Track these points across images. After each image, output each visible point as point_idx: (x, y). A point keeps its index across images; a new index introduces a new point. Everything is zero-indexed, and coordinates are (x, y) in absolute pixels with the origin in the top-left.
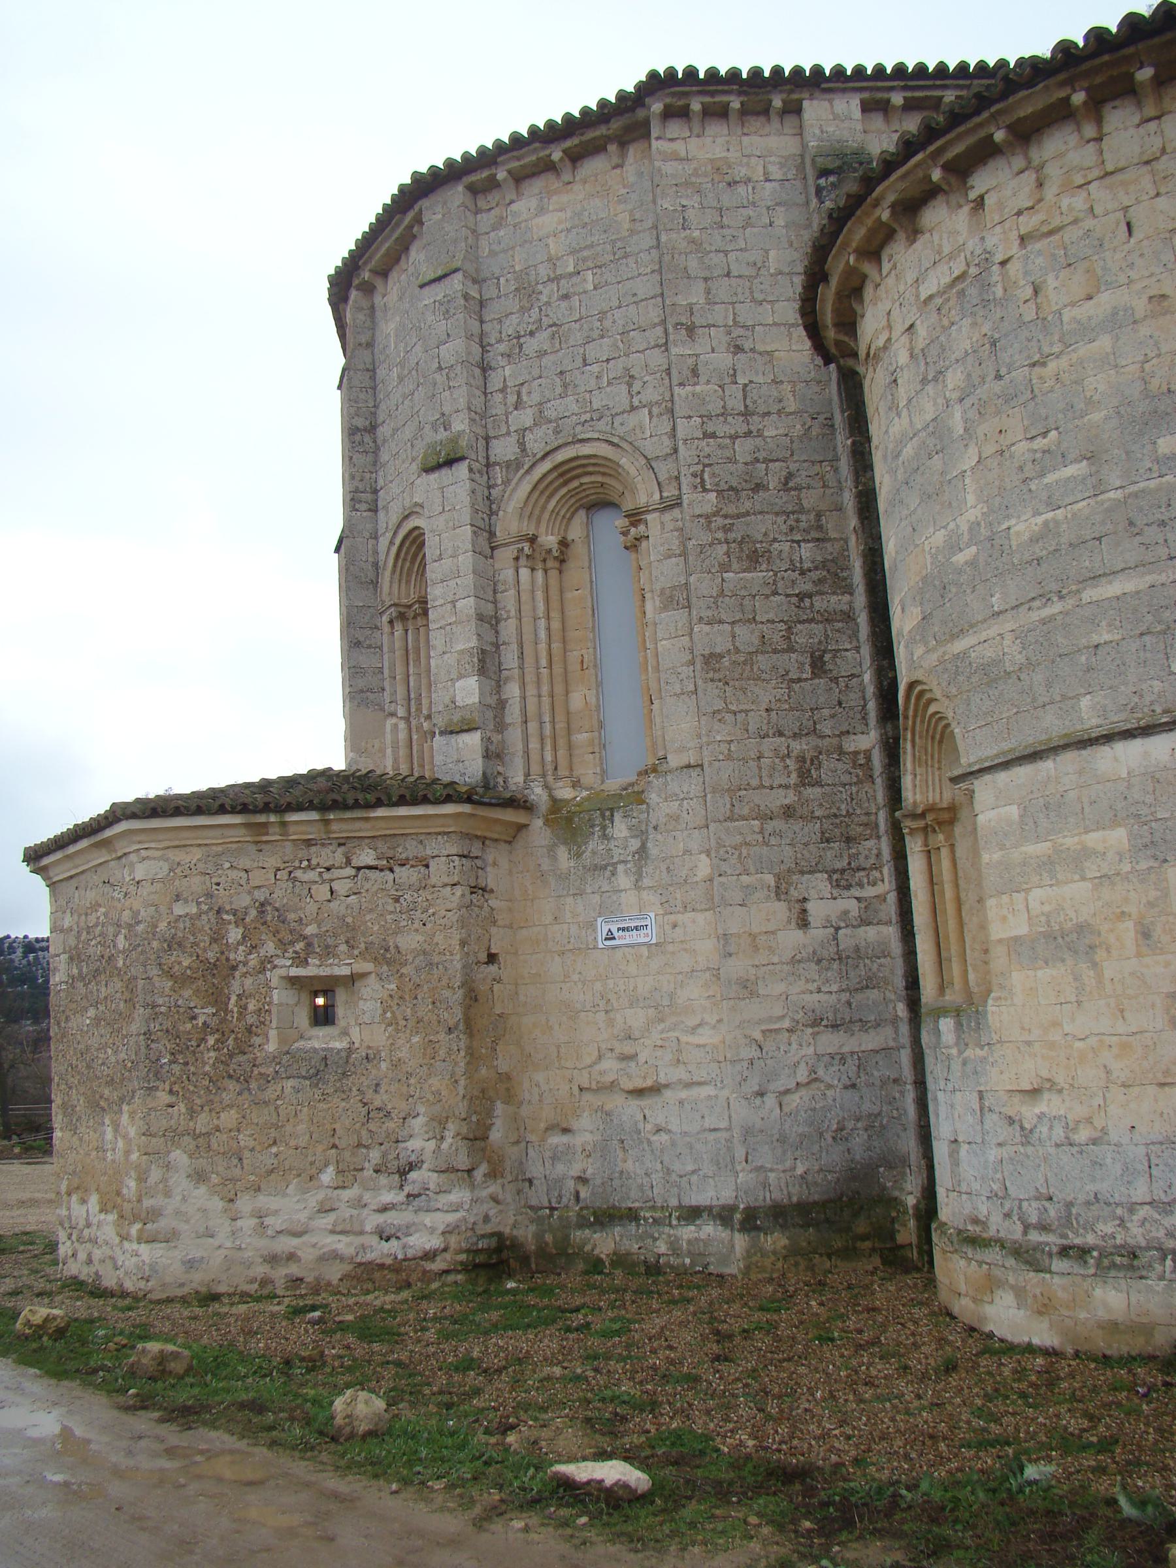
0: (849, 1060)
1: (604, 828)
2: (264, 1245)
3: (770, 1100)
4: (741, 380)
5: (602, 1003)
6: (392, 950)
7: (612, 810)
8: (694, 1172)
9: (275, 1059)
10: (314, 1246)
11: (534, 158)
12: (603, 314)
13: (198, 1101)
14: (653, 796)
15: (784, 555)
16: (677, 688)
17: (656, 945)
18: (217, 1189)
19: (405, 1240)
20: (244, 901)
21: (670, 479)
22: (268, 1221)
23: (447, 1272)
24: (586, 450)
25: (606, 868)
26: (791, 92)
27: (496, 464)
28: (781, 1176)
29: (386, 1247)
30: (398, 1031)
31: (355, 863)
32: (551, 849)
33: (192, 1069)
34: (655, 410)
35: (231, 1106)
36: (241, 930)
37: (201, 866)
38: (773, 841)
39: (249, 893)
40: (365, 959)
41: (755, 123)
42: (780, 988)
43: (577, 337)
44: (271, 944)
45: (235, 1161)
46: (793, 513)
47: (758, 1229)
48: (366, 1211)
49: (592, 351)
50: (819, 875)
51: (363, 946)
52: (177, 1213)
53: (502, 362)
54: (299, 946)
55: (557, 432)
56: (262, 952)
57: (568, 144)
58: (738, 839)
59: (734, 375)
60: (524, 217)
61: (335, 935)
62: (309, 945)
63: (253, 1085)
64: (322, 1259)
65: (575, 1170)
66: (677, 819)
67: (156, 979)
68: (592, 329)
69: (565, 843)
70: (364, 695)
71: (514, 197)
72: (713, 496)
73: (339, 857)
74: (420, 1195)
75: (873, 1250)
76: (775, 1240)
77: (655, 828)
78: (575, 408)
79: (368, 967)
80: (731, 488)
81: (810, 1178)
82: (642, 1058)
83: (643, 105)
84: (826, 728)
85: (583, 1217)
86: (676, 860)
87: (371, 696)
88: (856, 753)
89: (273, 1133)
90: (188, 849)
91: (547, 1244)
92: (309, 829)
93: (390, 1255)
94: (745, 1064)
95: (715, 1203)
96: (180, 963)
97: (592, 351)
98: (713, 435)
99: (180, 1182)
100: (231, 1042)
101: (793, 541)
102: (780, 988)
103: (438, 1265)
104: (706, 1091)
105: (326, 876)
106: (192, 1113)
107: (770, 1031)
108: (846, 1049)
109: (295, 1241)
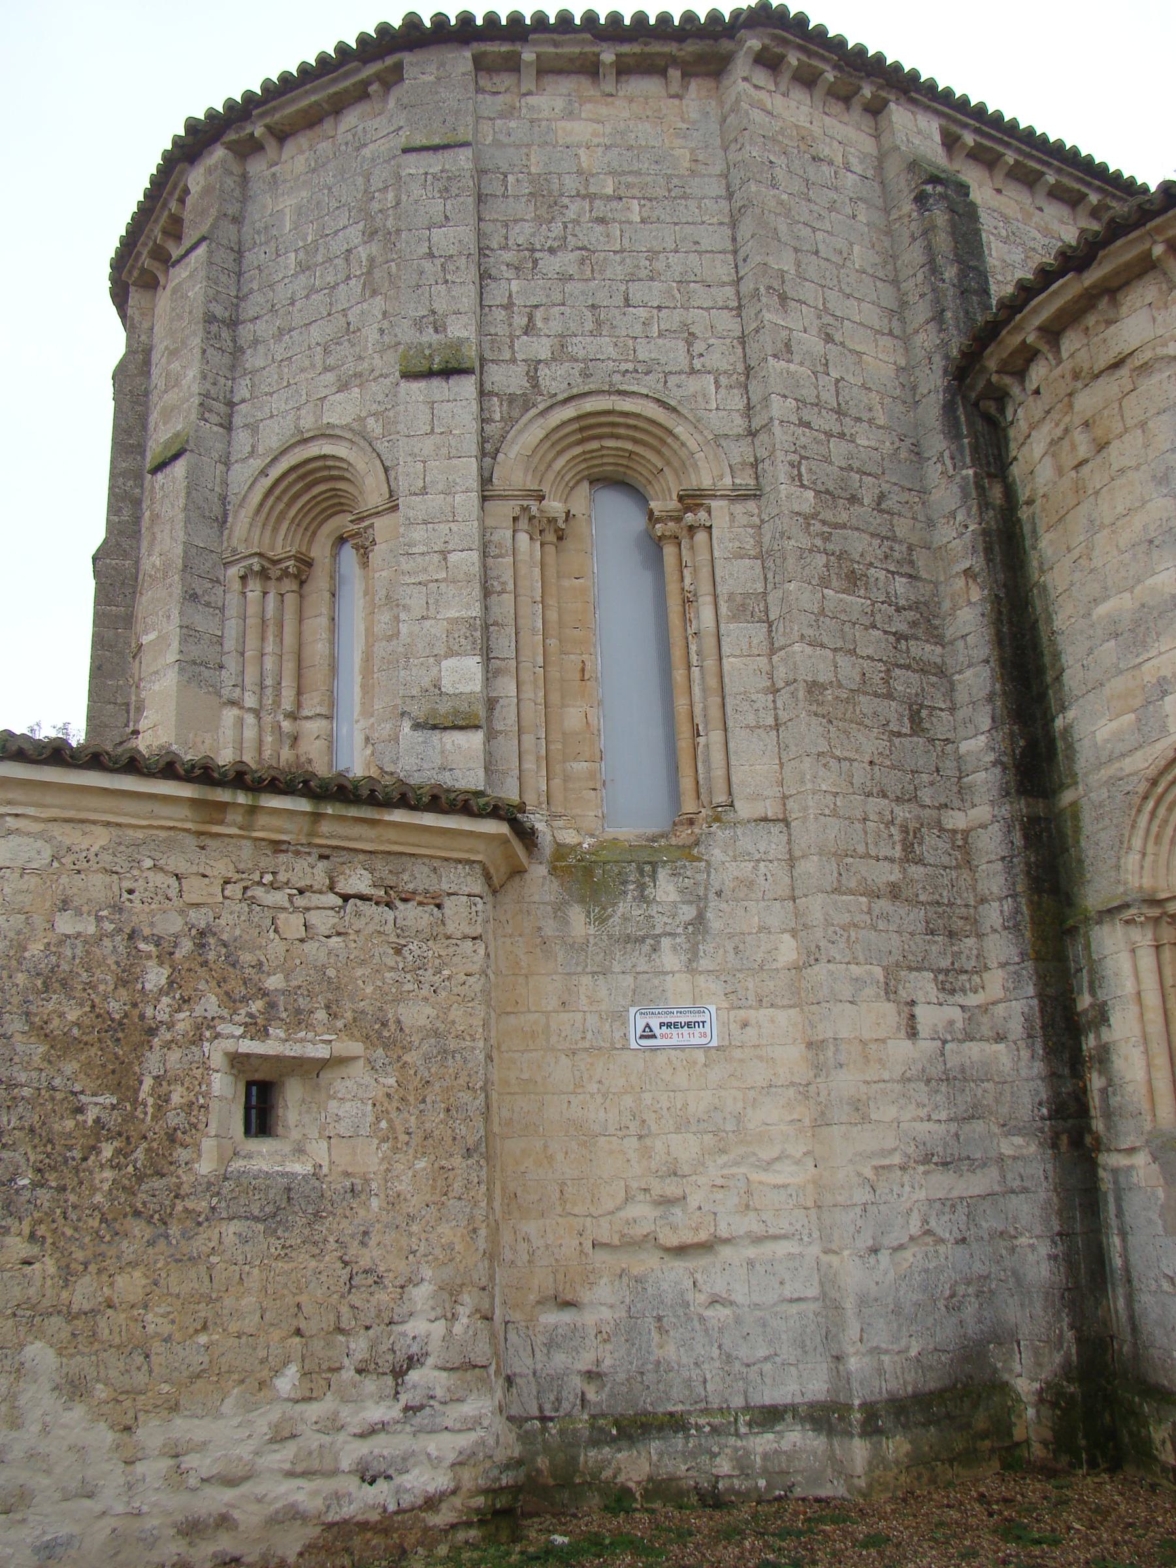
0: (959, 1207)
1: (642, 887)
2: (179, 1504)
3: (884, 1257)
4: (835, 374)
5: (634, 1127)
6: (392, 1026)
7: (654, 865)
8: (766, 1359)
9: (210, 1187)
10: (259, 1500)
11: (577, 50)
12: (652, 255)
13: (79, 1255)
14: (717, 852)
15: (881, 585)
16: (751, 719)
17: (717, 1049)
18: (105, 1409)
19: (398, 1480)
20: (172, 924)
21: (743, 463)
22: (190, 1461)
23: (453, 1527)
24: (627, 405)
25: (644, 940)
26: (880, 87)
27: (491, 394)
28: (884, 1358)
29: (381, 1493)
30: (395, 1150)
31: (343, 887)
32: (559, 909)
33: (73, 1198)
34: (723, 380)
35: (134, 1264)
36: (166, 972)
37: (106, 858)
38: (881, 925)
39: (182, 912)
40: (352, 1036)
41: (837, 108)
42: (891, 1112)
43: (617, 270)
44: (213, 999)
45: (139, 1360)
46: (888, 538)
47: (879, 1431)
48: (342, 1437)
49: (637, 291)
50: (925, 973)
51: (349, 1015)
52: (32, 1456)
53: (510, 274)
54: (256, 1006)
55: (586, 375)
56: (199, 1011)
57: (626, 48)
58: (846, 918)
59: (826, 365)
60: (545, 114)
61: (310, 995)
62: (272, 1005)
63: (174, 1230)
64: (274, 1521)
65: (585, 1361)
66: (751, 885)
67: (18, 1037)
68: (637, 266)
69: (582, 901)
70: (197, 669)
71: (533, 88)
72: (810, 494)
73: (319, 877)
74: (421, 1407)
75: (993, 1450)
76: (897, 1446)
77: (719, 894)
78: (611, 351)
79: (355, 1048)
80: (827, 492)
81: (924, 1361)
82: (693, 1201)
83: (732, 37)
84: (926, 796)
85: (601, 1430)
86: (748, 938)
87: (206, 673)
88: (954, 832)
89: (204, 1311)
90: (89, 828)
91: (539, 1471)
92: (287, 825)
93: (373, 1507)
94: (858, 1210)
95: (798, 1400)
96: (62, 1015)
97: (637, 291)
98: (808, 425)
99: (39, 1399)
100: (140, 1154)
101: (888, 571)
102: (891, 1112)
103: (440, 1519)
104: (782, 1248)
105: (300, 901)
106: (67, 1275)
107: (883, 1167)
108: (955, 1194)
109: (229, 1494)
